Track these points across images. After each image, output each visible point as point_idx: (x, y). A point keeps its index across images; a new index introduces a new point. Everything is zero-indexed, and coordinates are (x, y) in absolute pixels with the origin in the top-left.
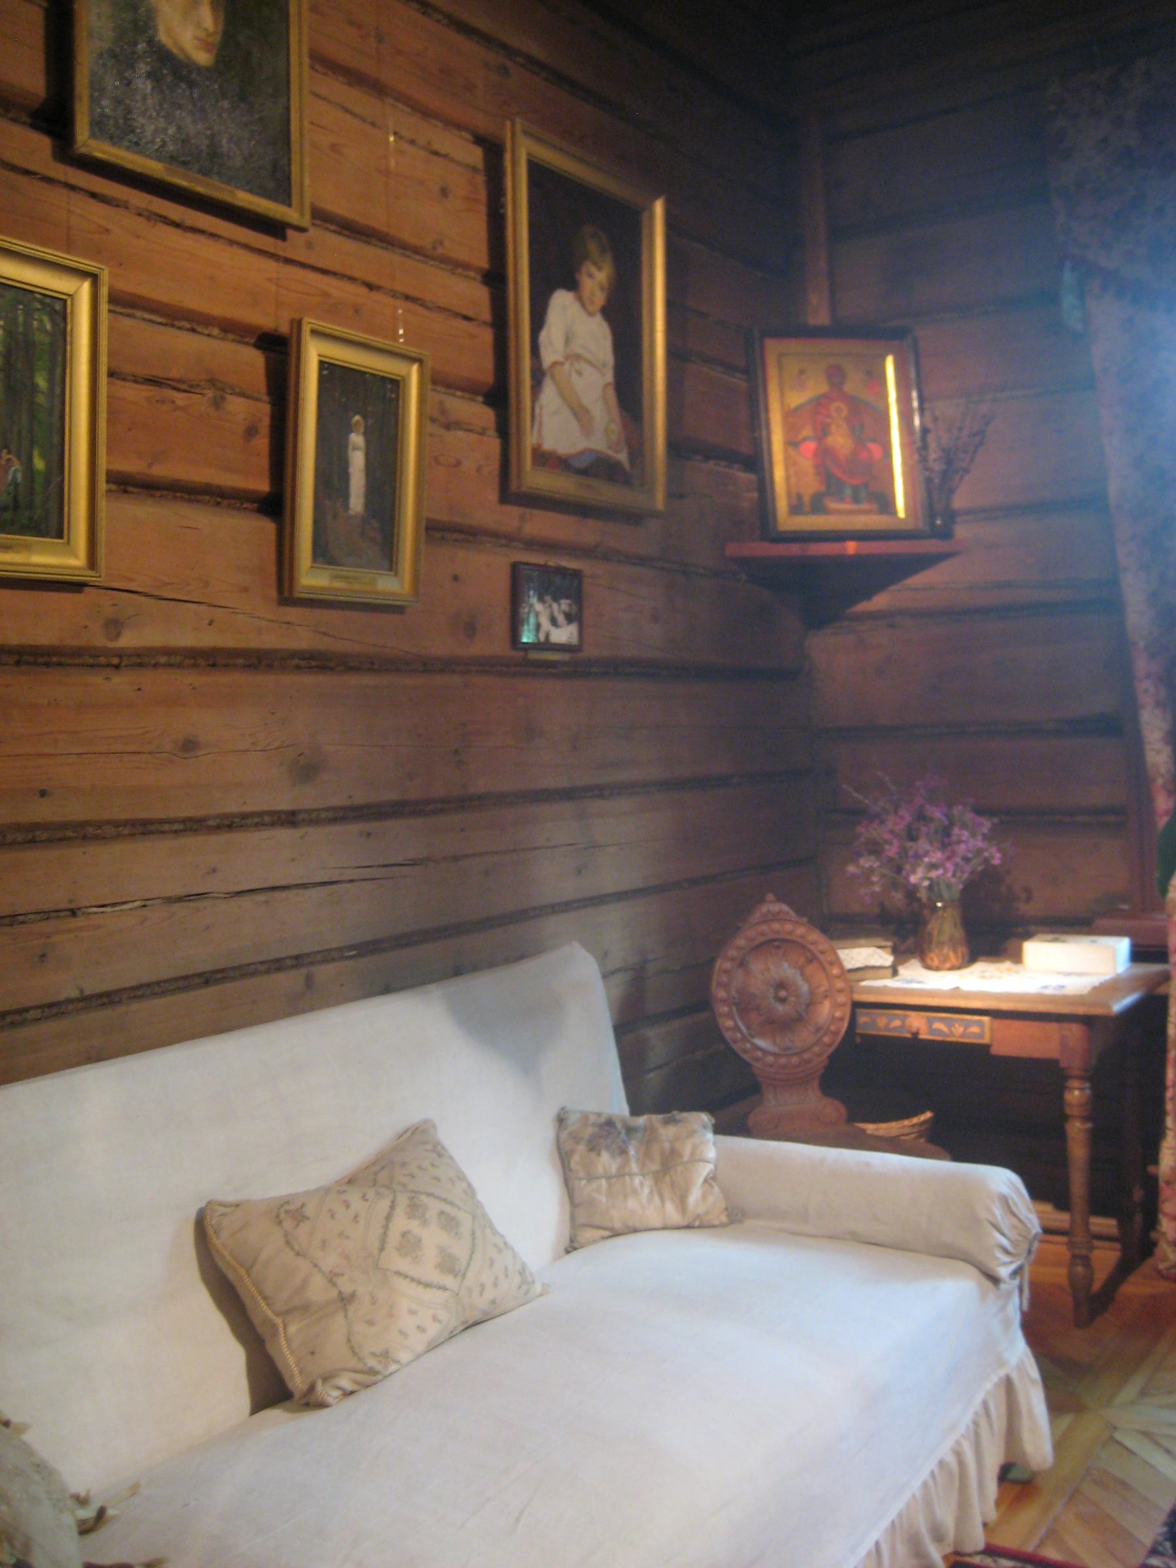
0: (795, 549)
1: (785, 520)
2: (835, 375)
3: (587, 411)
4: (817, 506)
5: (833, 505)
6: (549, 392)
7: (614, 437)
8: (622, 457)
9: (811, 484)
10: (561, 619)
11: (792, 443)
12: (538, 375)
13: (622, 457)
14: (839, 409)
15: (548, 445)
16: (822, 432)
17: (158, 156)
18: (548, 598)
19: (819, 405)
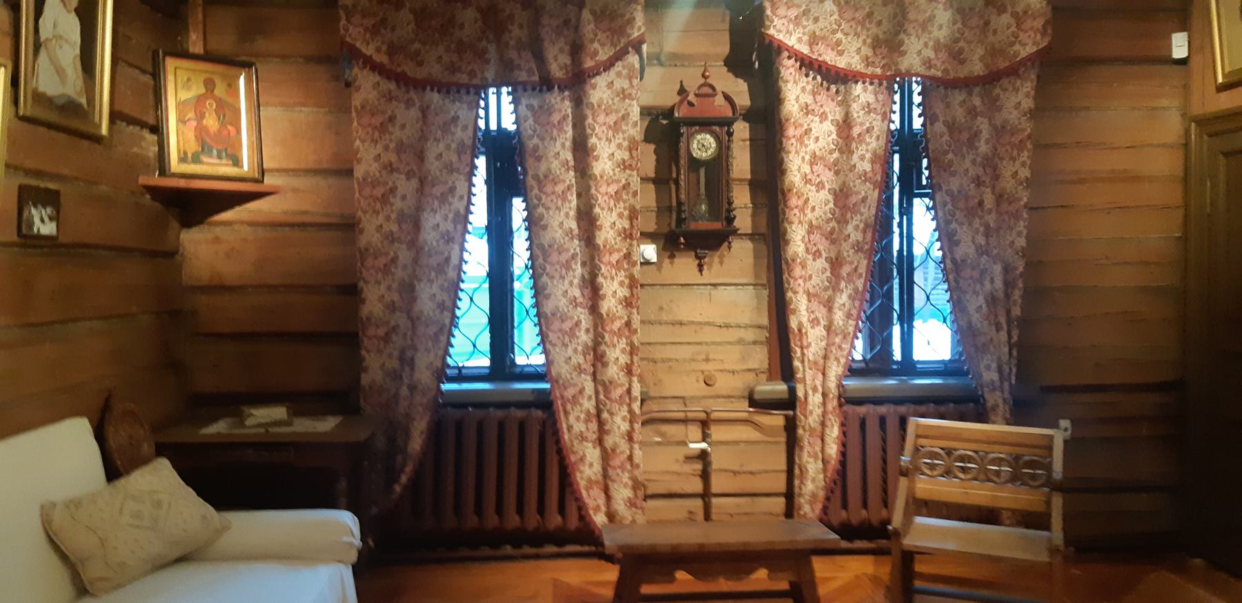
0: (182, 183)
1: (175, 165)
2: (209, 85)
3: (63, 70)
4: (196, 160)
5: (205, 159)
6: (43, 56)
7: (78, 88)
8: (84, 101)
9: (192, 147)
10: (46, 219)
11: (181, 120)
12: (37, 46)
13: (84, 101)
14: (211, 105)
15: (41, 89)
16: (200, 116)
17: (670, 217)
18: (40, 207)
19: (200, 100)
